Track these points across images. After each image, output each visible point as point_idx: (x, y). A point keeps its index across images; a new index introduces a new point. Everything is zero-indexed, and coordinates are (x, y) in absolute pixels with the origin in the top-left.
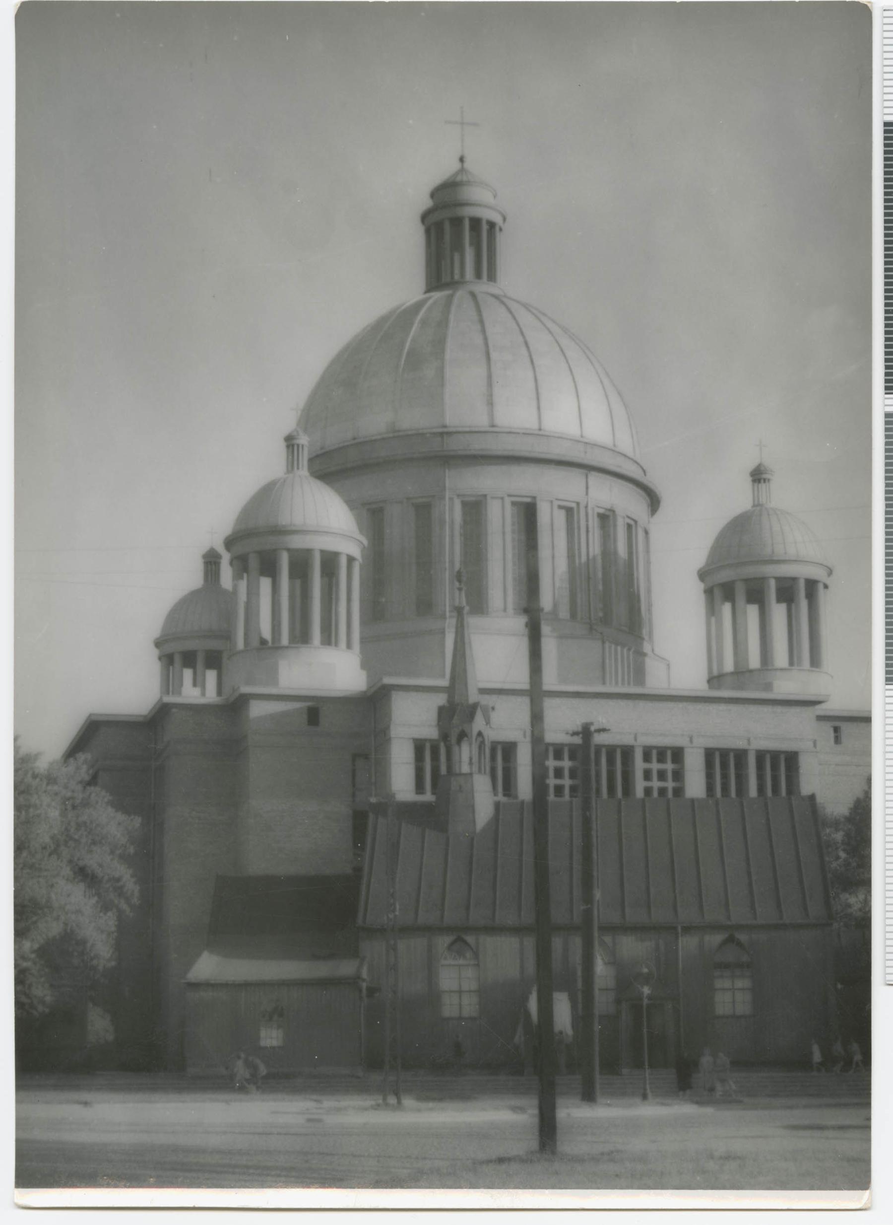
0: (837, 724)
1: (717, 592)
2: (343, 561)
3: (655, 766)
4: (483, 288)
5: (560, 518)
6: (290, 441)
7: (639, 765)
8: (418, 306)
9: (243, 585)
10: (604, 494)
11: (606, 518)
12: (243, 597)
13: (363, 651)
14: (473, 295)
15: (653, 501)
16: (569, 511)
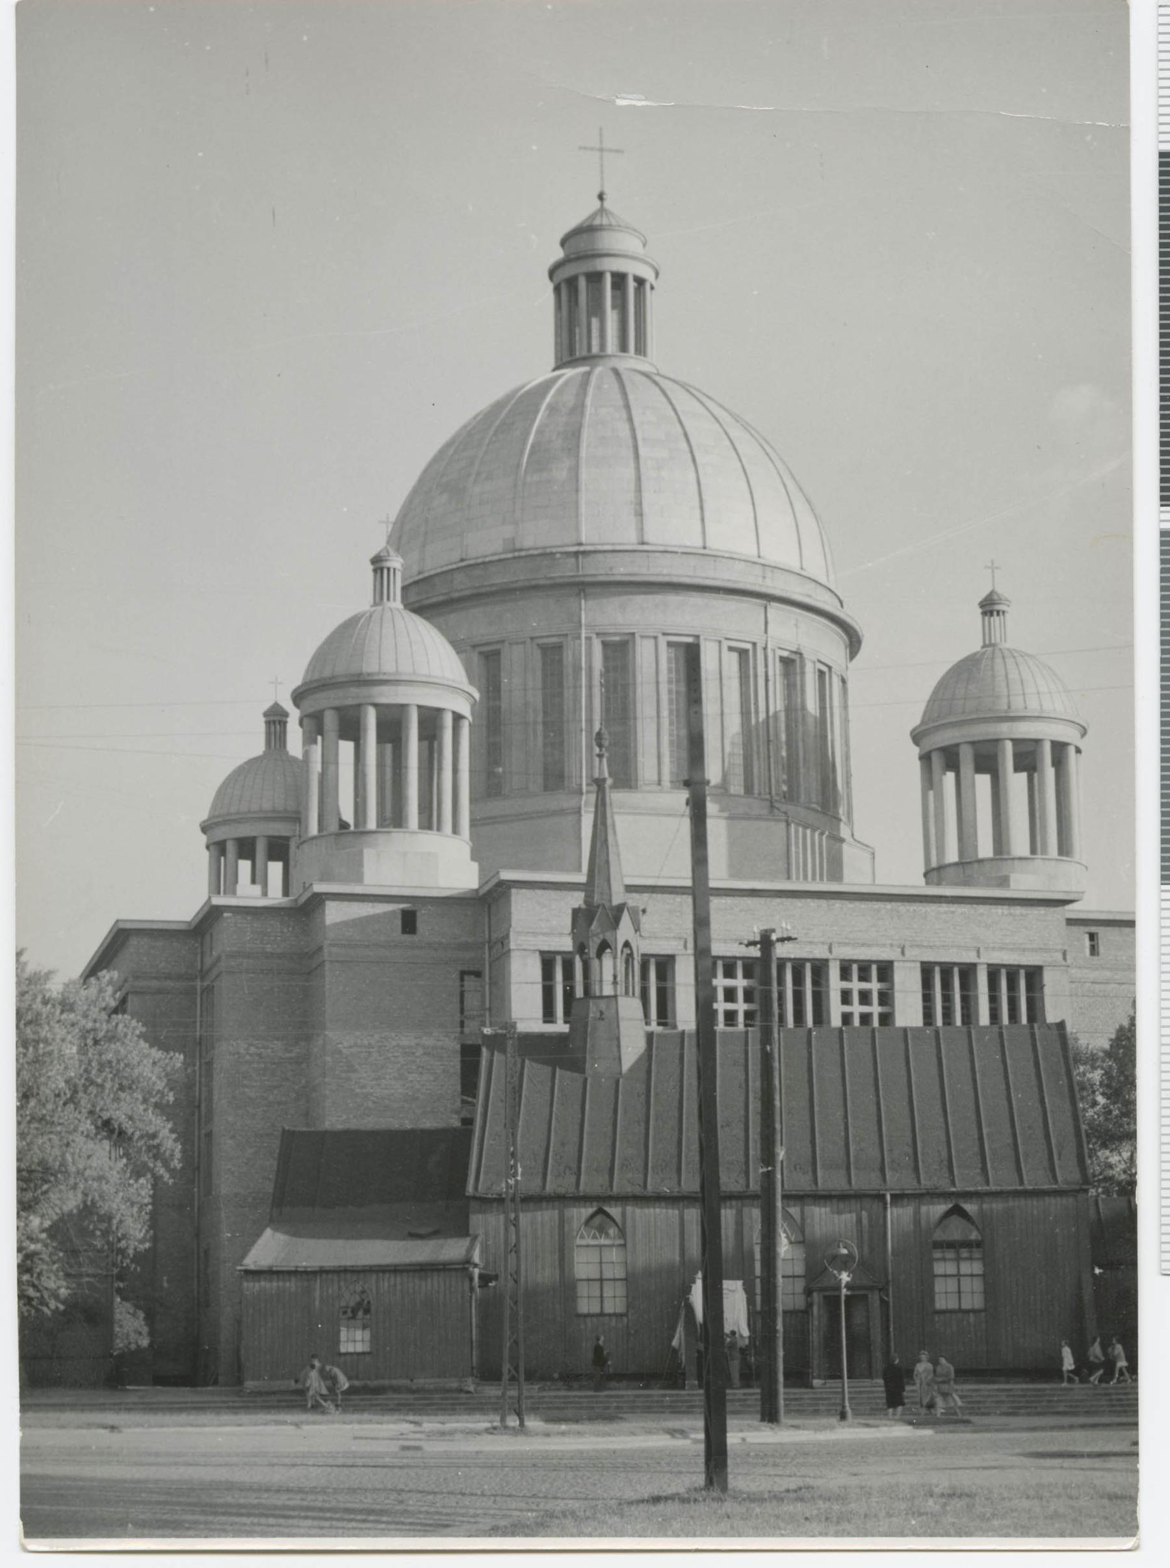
2: (448, 720)
3: (856, 985)
4: (629, 363)
5: (731, 662)
7: (835, 984)
8: (554, 380)
11: (791, 664)
14: (616, 372)
15: (853, 641)
16: (743, 653)
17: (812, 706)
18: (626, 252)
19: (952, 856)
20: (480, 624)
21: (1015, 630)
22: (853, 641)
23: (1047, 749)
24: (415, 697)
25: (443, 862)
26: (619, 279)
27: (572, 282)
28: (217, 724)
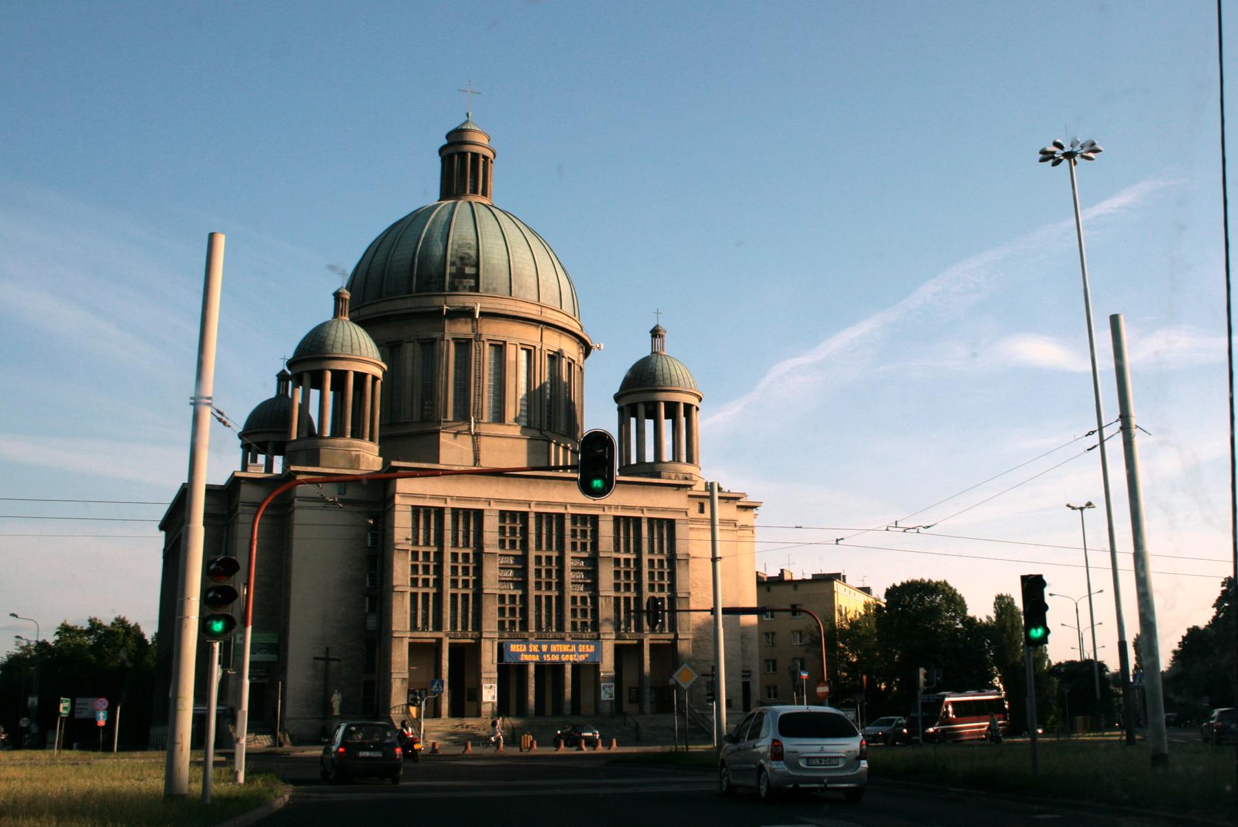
0: (702, 500)
1: (626, 409)
2: (370, 378)
3: (579, 527)
4: (479, 198)
5: (523, 355)
6: (337, 296)
7: (568, 525)
8: (435, 207)
9: (299, 391)
10: (554, 342)
11: (555, 357)
12: (298, 399)
13: (380, 444)
14: (470, 203)
15: (587, 349)
16: (529, 352)
17: (565, 378)
18: (480, 141)
19: (633, 461)
20: (392, 334)
21: (670, 347)
22: (587, 349)
23: (682, 406)
24: (353, 367)
25: (369, 456)
26: (475, 156)
27: (451, 156)
28: (250, 382)
